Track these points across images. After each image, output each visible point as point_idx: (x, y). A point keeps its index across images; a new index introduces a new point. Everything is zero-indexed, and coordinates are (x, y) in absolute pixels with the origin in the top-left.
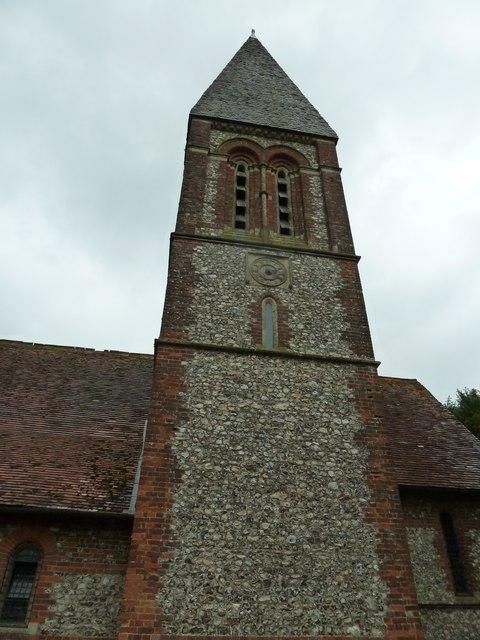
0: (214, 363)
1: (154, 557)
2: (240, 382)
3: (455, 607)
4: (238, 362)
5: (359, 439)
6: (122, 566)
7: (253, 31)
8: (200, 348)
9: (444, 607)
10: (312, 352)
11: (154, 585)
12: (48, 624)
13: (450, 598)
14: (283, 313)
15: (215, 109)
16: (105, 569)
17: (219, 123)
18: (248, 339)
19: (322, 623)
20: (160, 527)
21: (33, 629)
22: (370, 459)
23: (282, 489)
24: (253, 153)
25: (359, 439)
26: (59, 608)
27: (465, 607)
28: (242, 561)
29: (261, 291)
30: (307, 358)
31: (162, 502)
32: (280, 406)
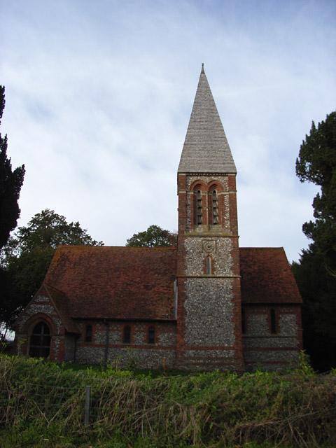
0: (193, 282)
1: (182, 331)
2: (200, 286)
3: (270, 337)
4: (199, 280)
5: (232, 301)
6: (176, 331)
7: (23, 166)
8: (189, 277)
9: (267, 337)
10: (221, 275)
11: (183, 337)
12: (160, 344)
13: (268, 334)
14: (213, 261)
15: (182, 171)
16: (171, 331)
17: (189, 174)
18: (202, 273)
19: (219, 344)
20: (183, 325)
21: (157, 345)
22: (236, 305)
23: (211, 315)
24: (214, 185)
25: (232, 301)
26: (162, 340)
27: (273, 337)
28: (202, 332)
29: (206, 255)
30: (219, 277)
31: (183, 319)
32: (211, 293)
